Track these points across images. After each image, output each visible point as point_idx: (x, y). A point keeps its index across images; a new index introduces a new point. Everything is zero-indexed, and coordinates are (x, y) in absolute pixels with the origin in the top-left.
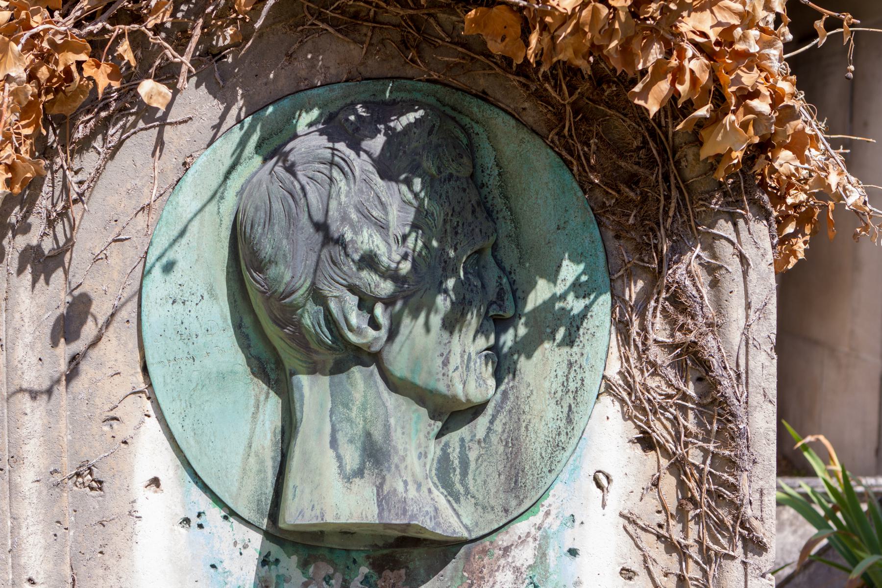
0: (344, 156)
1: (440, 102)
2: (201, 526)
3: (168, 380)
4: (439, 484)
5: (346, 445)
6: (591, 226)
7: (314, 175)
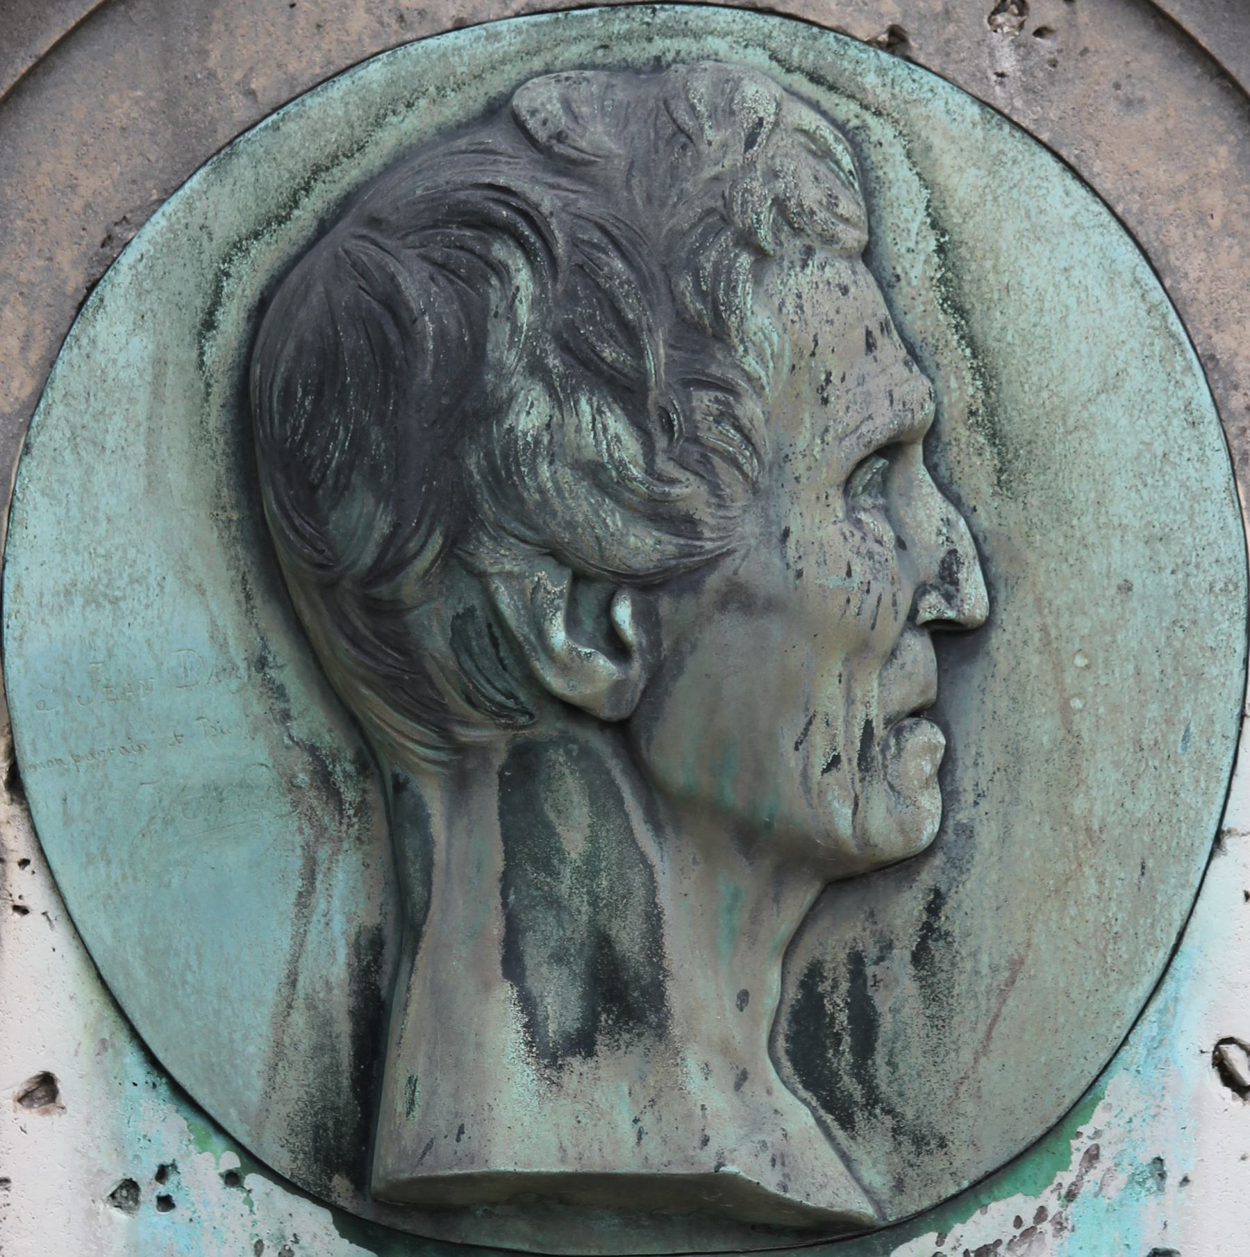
0: (525, 207)
1: (779, 61)
2: (166, 1203)
3: (75, 807)
4: (796, 1079)
5: (544, 969)
6: (1188, 381)
7: (449, 256)
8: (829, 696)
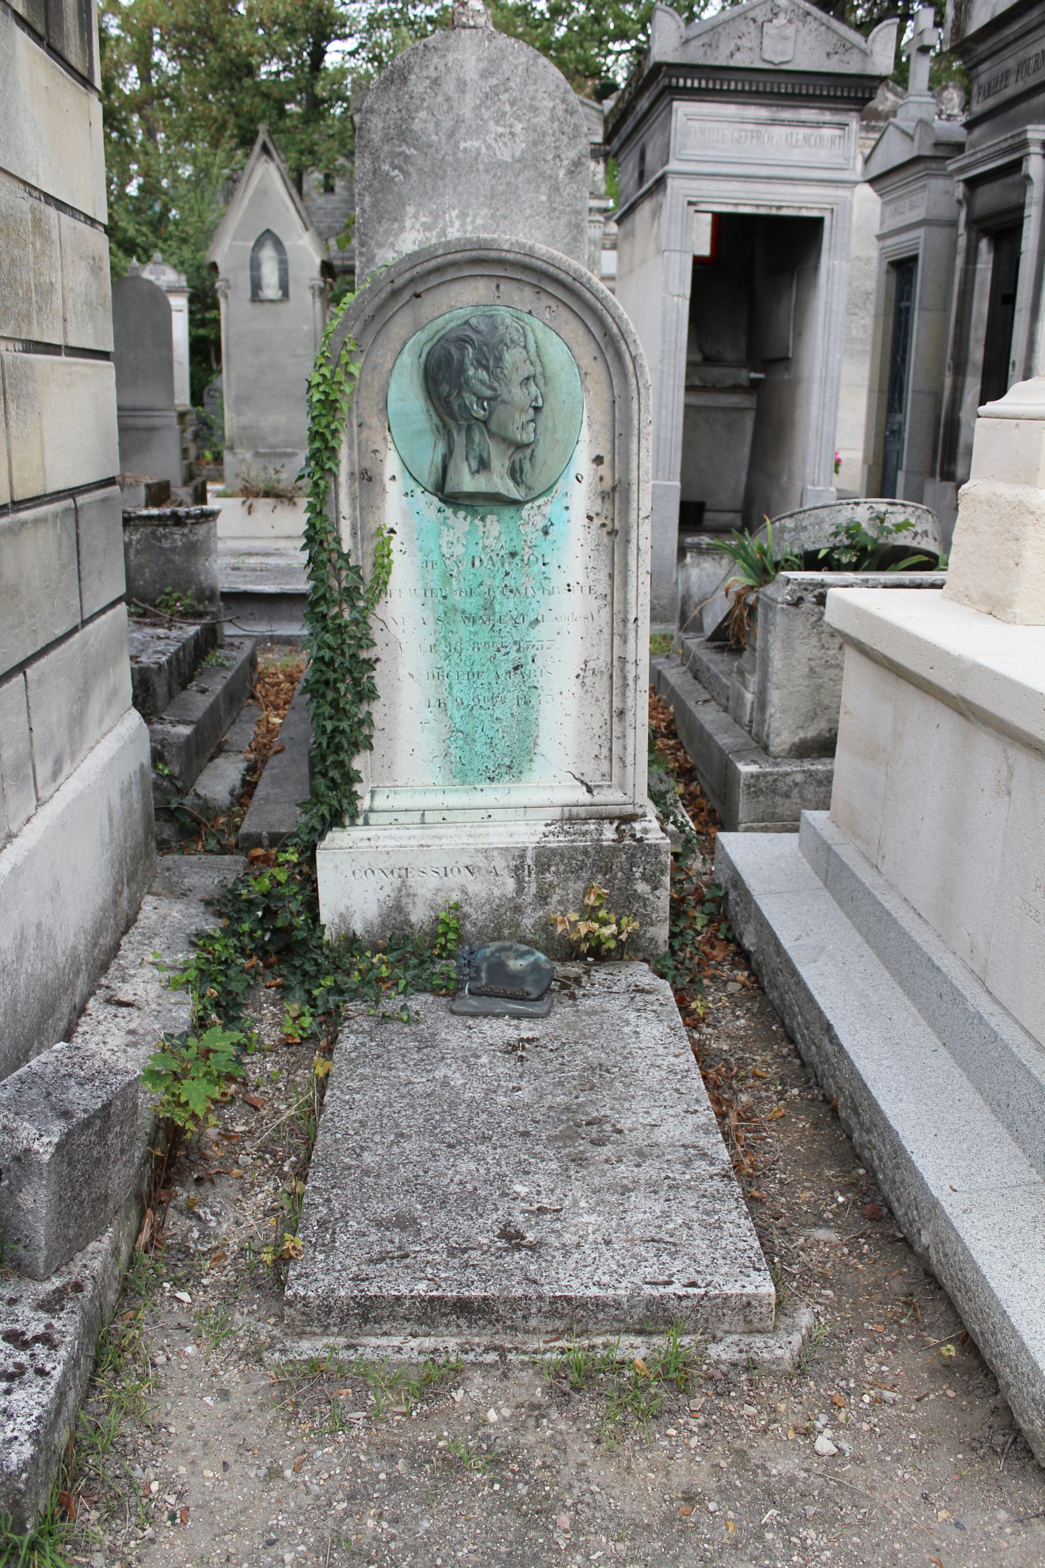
8: (517, 417)
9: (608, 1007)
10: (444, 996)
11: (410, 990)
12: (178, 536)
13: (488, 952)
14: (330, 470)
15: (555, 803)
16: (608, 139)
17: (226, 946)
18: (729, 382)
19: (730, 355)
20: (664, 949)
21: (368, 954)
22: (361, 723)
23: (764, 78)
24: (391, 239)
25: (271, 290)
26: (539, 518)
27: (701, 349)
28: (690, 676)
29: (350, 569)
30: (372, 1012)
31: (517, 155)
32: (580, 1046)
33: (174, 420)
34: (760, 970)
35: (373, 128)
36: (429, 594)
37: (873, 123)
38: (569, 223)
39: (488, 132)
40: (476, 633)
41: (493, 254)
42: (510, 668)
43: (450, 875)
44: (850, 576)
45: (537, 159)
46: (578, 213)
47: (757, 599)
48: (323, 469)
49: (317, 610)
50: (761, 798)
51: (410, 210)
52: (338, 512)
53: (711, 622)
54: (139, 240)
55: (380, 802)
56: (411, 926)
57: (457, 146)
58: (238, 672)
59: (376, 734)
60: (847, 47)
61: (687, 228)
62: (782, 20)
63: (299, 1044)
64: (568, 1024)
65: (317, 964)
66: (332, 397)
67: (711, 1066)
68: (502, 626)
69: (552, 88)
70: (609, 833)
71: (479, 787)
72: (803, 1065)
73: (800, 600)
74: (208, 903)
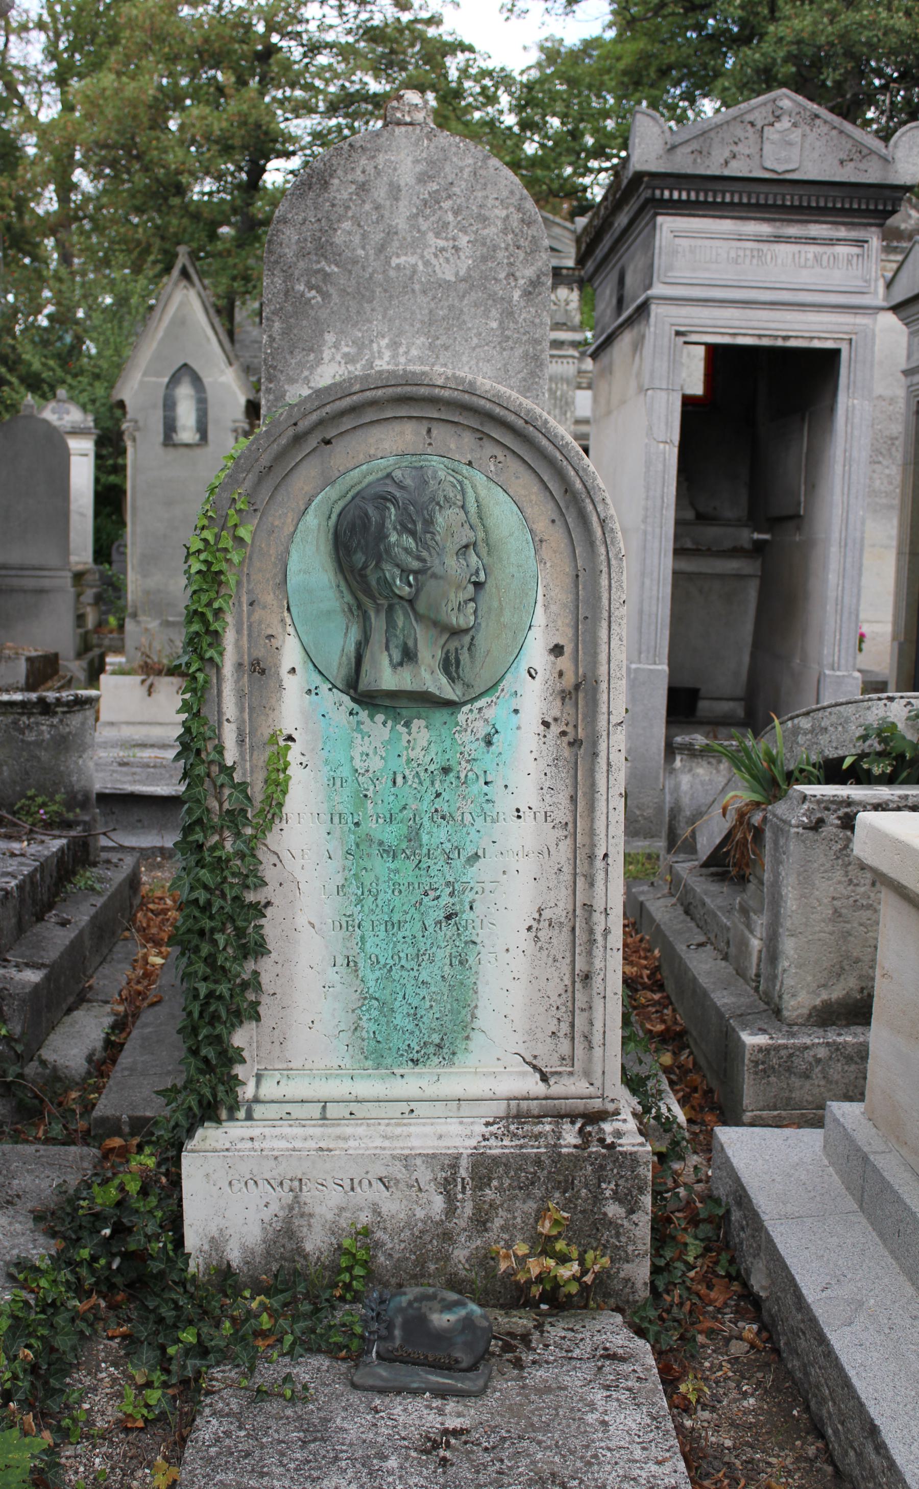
8: (452, 596)
9: (566, 1380)
10: (344, 1359)
11: (298, 1350)
12: (45, 728)
13: (404, 1300)
14: (211, 659)
15: (498, 1095)
16: (581, 261)
17: (54, 1281)
18: (728, 544)
19: (728, 513)
20: (644, 1293)
21: (247, 1294)
22: (245, 985)
23: (764, 188)
24: (306, 373)
25: (187, 433)
26: (479, 724)
27: (693, 505)
28: (680, 910)
29: (235, 786)
30: (245, 1383)
31: (462, 273)
32: (525, 1444)
33: (69, 581)
34: (774, 1325)
35: (286, 241)
36: (336, 819)
37: (895, 244)
38: (526, 354)
39: (426, 246)
40: (397, 871)
41: (423, 391)
42: (441, 915)
43: (358, 1190)
44: (883, 792)
45: (486, 278)
46: (537, 342)
47: (765, 819)
48: (202, 658)
49: (190, 839)
50: (773, 1079)
51: (330, 338)
52: (220, 713)
53: (707, 842)
54: (44, 375)
55: (268, 1089)
56: (306, 1257)
57: (388, 263)
58: (111, 898)
59: (264, 999)
60: (864, 153)
61: (674, 363)
62: (785, 123)
63: (141, 1429)
64: (510, 1408)
65: (177, 1307)
66: (215, 568)
67: (708, 1475)
68: (431, 862)
69: (505, 193)
70: (570, 1136)
71: (398, 1071)
72: (838, 1473)
73: (820, 822)
74: (38, 1217)
